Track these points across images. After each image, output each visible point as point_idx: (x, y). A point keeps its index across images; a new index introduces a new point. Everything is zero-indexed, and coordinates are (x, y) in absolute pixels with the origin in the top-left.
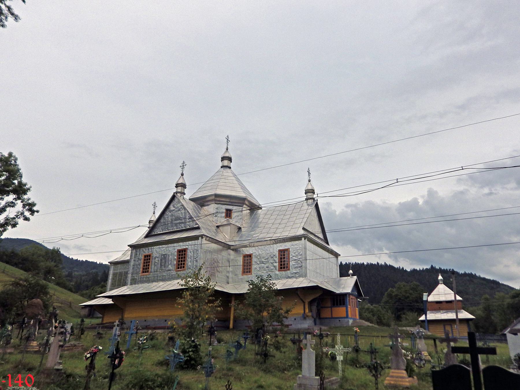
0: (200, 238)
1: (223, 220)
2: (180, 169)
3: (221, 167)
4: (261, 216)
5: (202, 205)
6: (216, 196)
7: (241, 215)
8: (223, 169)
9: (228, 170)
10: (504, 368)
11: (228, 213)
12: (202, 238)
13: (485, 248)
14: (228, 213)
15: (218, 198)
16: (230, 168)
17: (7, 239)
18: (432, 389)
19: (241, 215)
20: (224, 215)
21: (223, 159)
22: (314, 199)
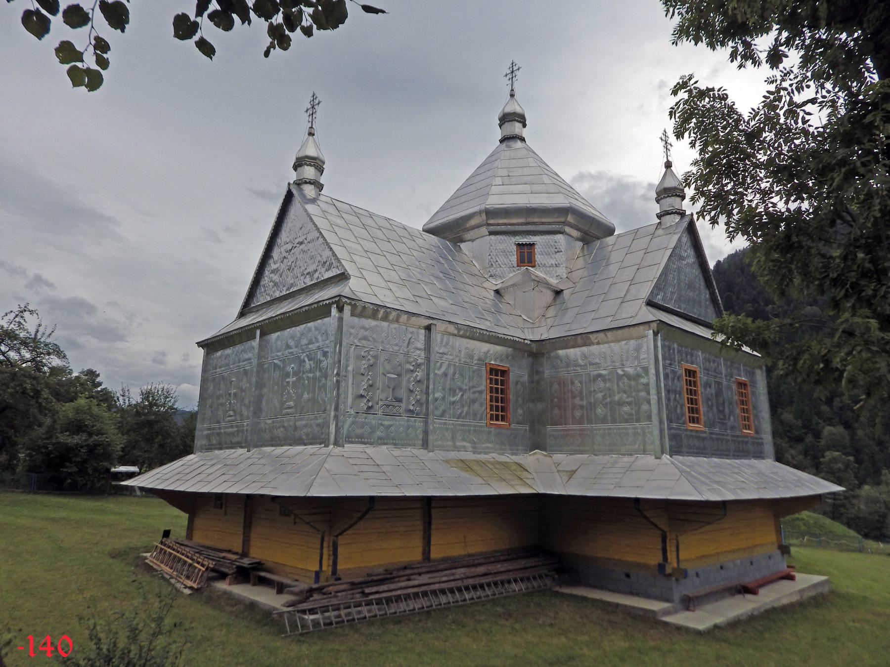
0: (334, 311)
1: (512, 275)
2: (506, 81)
3: (501, 141)
4: (616, 256)
5: (458, 240)
6: (491, 213)
7: (557, 256)
8: (504, 144)
9: (519, 144)
10: (298, 328)
11: (526, 254)
12: (340, 309)
13: (641, 327)
14: (526, 254)
15: (499, 221)
16: (523, 140)
17: (715, 267)
18: (121, 224)
19: (557, 256)
20: (514, 259)
21: (505, 119)
22: (682, 214)
